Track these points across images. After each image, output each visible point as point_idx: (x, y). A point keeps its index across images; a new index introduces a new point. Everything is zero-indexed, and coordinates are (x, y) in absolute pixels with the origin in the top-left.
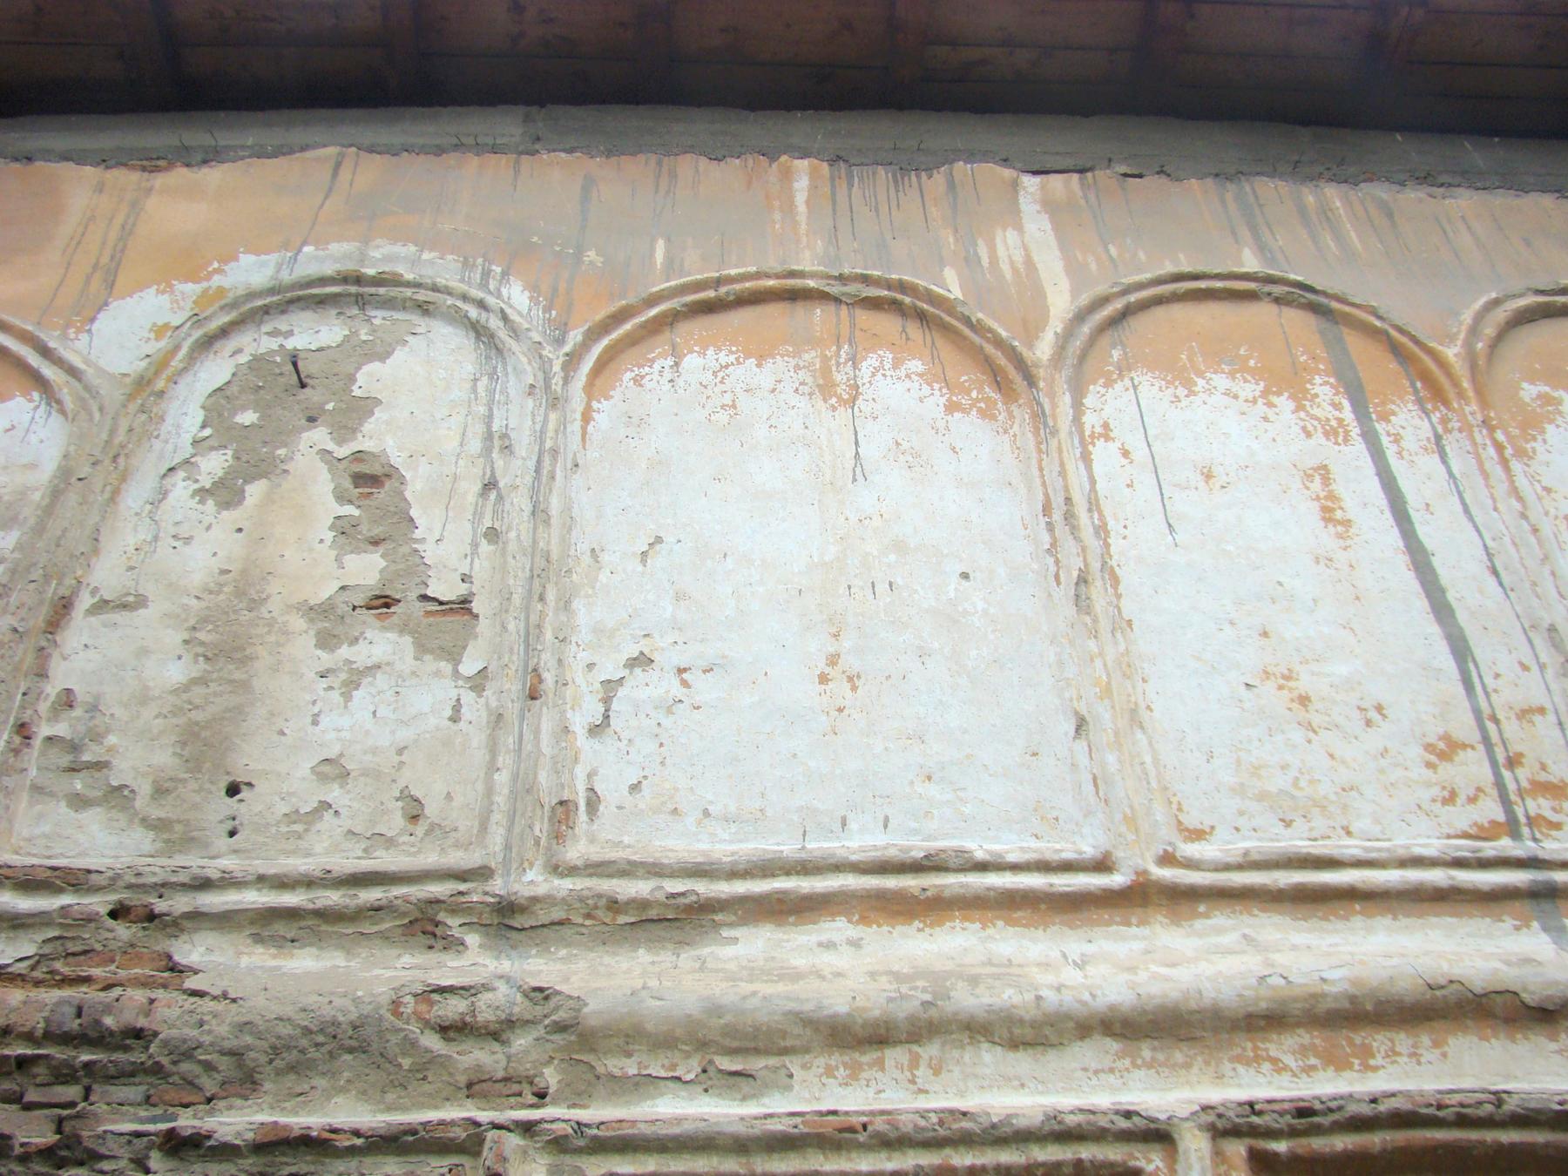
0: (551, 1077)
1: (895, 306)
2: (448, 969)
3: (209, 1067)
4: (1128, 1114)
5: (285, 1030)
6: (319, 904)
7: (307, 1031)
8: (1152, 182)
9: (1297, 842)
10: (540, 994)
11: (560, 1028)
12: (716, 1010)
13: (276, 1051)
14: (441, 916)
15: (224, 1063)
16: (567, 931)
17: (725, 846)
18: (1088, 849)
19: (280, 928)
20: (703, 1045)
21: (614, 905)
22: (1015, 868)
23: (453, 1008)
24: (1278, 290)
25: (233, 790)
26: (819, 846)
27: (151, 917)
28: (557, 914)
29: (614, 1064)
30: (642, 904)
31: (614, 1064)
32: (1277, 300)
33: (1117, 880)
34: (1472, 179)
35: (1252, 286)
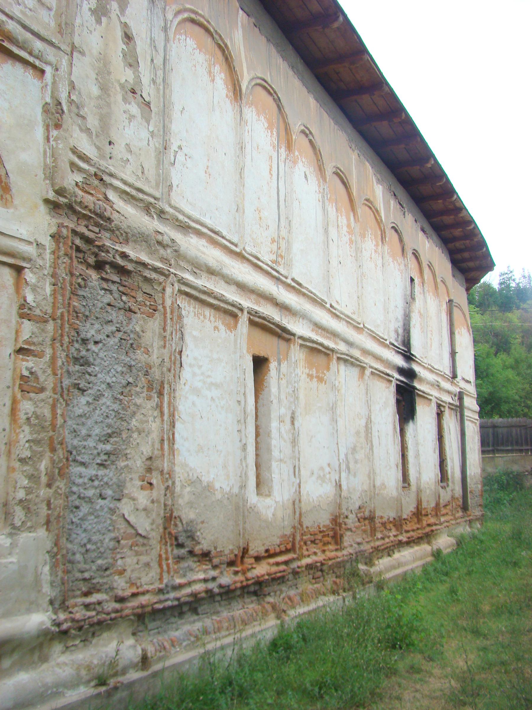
0: (173, 262)
1: (223, 51)
2: (162, 228)
3: (122, 234)
4: (240, 304)
5: (136, 231)
6: (132, 194)
7: (139, 233)
8: (257, 30)
9: (139, 185)
10: (173, 240)
11: (176, 251)
12: (196, 257)
13: (133, 235)
14: (151, 208)
15: (124, 235)
16: (168, 221)
17: (195, 214)
18: (235, 240)
19: (124, 196)
20: (193, 264)
21: (177, 220)
22: (227, 240)
23: (160, 238)
24: (276, 97)
25: (110, 143)
26: (203, 219)
27: (102, 180)
28: (168, 217)
29: (182, 264)
30: (181, 222)
31: (182, 264)
32: (274, 99)
33: (238, 250)
34: (302, 80)
35: (272, 92)
